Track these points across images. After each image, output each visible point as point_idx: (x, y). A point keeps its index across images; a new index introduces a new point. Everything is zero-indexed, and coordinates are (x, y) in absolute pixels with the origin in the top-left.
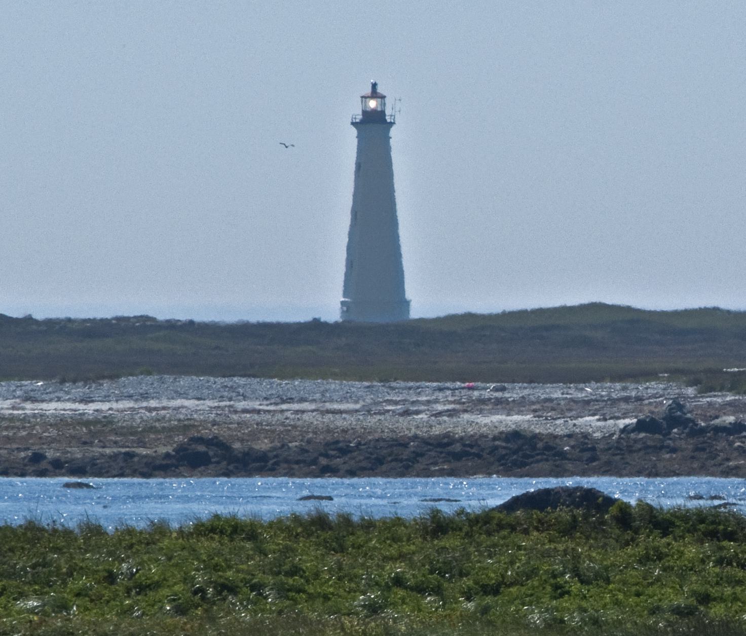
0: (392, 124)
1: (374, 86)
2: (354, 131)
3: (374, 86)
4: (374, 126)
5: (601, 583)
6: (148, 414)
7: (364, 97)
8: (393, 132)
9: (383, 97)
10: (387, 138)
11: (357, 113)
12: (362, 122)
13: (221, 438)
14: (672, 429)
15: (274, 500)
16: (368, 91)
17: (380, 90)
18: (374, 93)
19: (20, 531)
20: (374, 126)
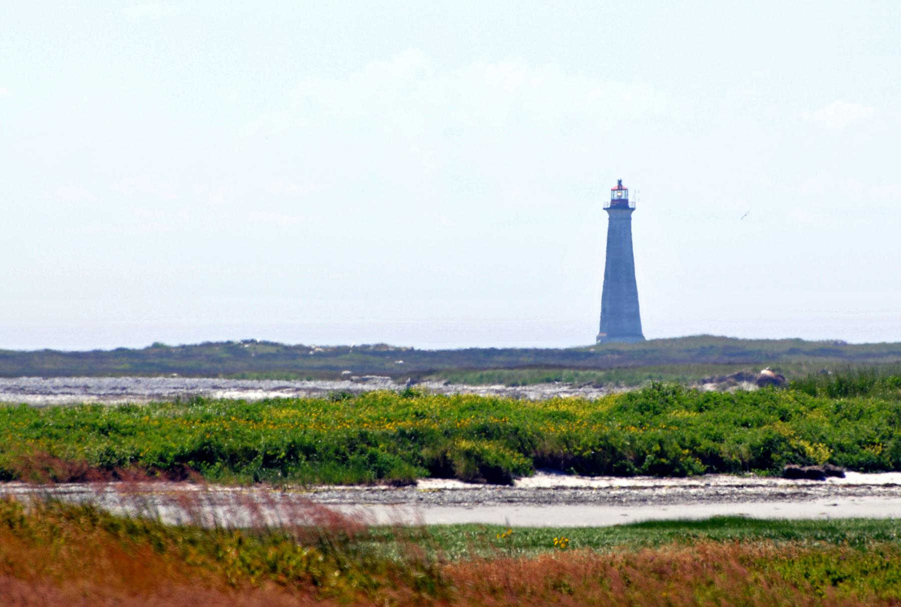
0: (633, 209)
1: (620, 182)
2: (606, 215)
3: (620, 182)
4: (620, 209)
5: (25, 523)
6: (680, 449)
7: (613, 190)
8: (634, 215)
9: (626, 190)
10: (629, 219)
11: (608, 202)
12: (612, 207)
13: (317, 349)
14: (668, 465)
15: (172, 386)
16: (616, 185)
17: (624, 184)
18: (620, 187)
19: (300, 481)
20: (620, 209)
